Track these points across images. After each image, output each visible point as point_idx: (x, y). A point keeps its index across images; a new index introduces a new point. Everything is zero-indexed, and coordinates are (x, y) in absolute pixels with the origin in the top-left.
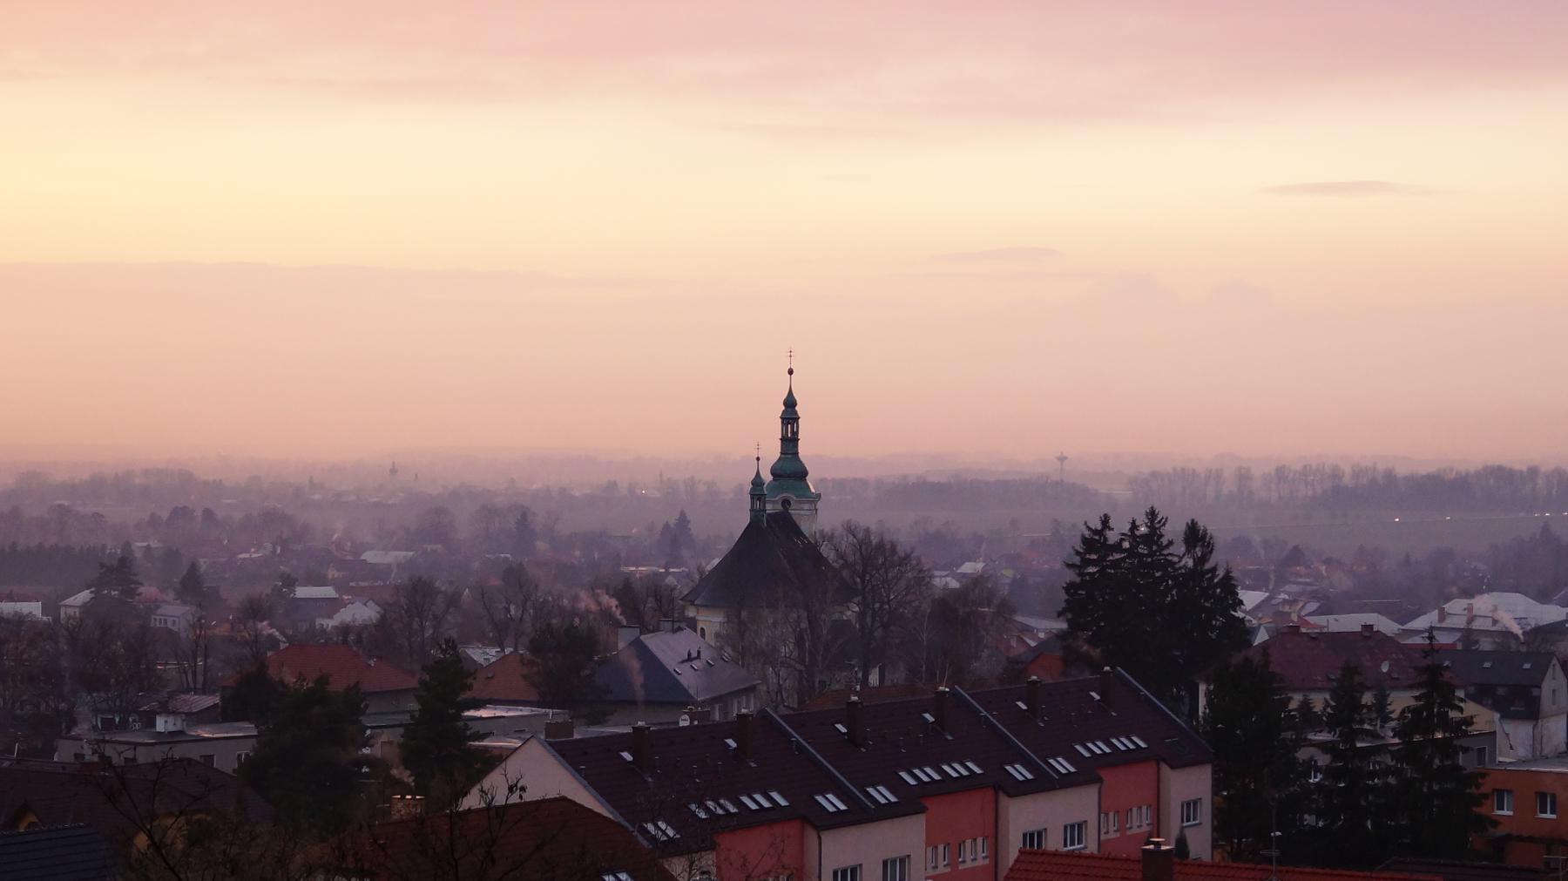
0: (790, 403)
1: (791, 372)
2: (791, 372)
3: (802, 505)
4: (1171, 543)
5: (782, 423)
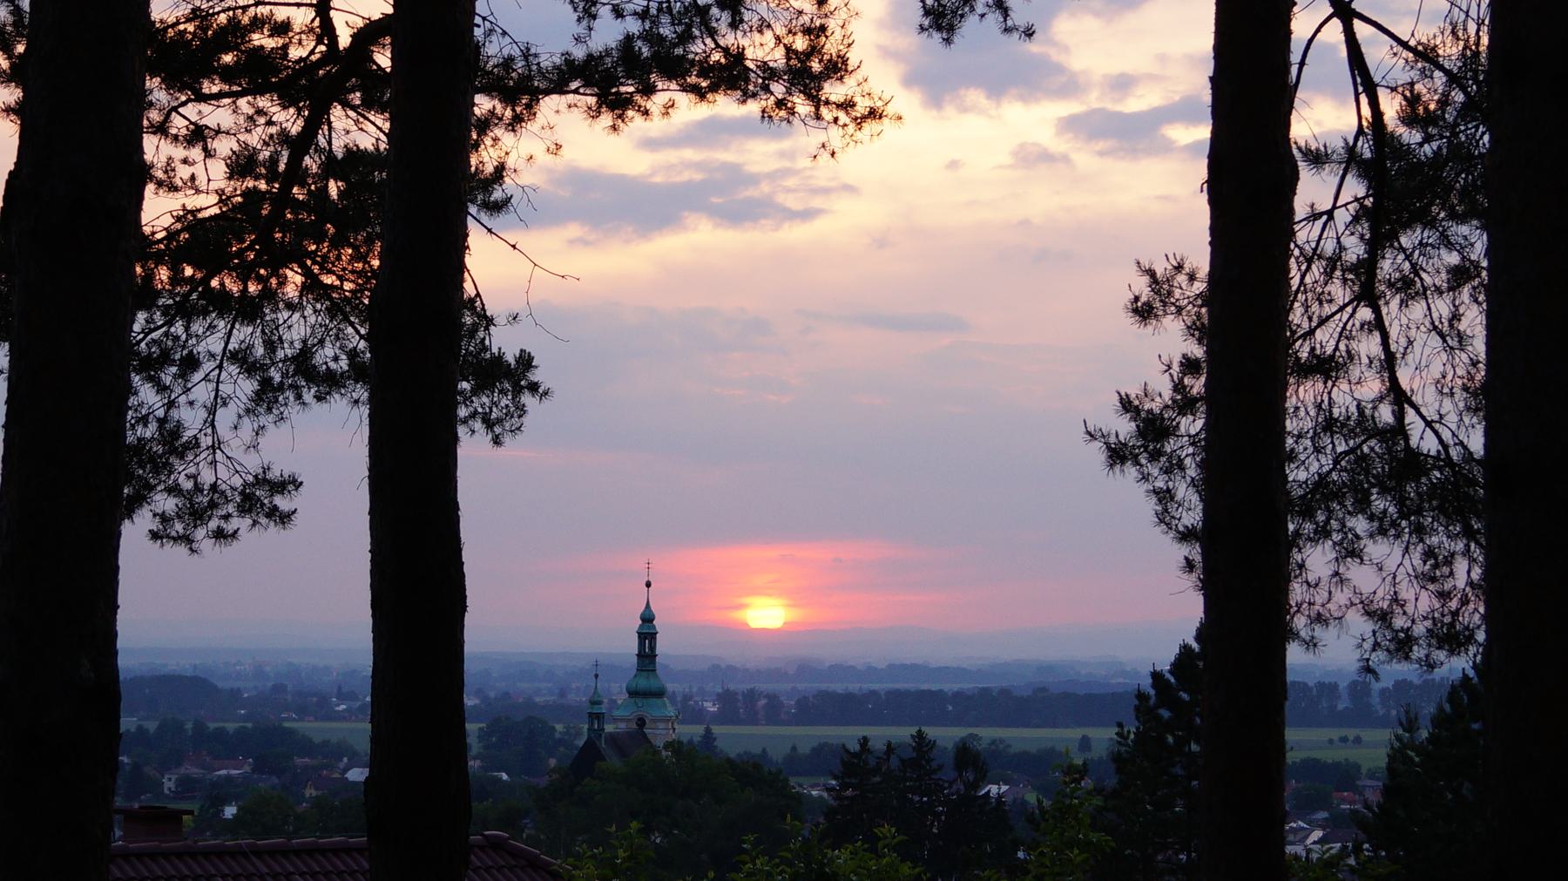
0: (648, 618)
1: (648, 585)
2: (648, 585)
3: (658, 724)
4: (940, 767)
5: (639, 637)
